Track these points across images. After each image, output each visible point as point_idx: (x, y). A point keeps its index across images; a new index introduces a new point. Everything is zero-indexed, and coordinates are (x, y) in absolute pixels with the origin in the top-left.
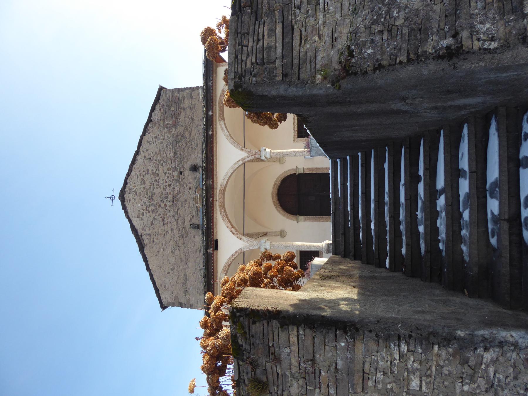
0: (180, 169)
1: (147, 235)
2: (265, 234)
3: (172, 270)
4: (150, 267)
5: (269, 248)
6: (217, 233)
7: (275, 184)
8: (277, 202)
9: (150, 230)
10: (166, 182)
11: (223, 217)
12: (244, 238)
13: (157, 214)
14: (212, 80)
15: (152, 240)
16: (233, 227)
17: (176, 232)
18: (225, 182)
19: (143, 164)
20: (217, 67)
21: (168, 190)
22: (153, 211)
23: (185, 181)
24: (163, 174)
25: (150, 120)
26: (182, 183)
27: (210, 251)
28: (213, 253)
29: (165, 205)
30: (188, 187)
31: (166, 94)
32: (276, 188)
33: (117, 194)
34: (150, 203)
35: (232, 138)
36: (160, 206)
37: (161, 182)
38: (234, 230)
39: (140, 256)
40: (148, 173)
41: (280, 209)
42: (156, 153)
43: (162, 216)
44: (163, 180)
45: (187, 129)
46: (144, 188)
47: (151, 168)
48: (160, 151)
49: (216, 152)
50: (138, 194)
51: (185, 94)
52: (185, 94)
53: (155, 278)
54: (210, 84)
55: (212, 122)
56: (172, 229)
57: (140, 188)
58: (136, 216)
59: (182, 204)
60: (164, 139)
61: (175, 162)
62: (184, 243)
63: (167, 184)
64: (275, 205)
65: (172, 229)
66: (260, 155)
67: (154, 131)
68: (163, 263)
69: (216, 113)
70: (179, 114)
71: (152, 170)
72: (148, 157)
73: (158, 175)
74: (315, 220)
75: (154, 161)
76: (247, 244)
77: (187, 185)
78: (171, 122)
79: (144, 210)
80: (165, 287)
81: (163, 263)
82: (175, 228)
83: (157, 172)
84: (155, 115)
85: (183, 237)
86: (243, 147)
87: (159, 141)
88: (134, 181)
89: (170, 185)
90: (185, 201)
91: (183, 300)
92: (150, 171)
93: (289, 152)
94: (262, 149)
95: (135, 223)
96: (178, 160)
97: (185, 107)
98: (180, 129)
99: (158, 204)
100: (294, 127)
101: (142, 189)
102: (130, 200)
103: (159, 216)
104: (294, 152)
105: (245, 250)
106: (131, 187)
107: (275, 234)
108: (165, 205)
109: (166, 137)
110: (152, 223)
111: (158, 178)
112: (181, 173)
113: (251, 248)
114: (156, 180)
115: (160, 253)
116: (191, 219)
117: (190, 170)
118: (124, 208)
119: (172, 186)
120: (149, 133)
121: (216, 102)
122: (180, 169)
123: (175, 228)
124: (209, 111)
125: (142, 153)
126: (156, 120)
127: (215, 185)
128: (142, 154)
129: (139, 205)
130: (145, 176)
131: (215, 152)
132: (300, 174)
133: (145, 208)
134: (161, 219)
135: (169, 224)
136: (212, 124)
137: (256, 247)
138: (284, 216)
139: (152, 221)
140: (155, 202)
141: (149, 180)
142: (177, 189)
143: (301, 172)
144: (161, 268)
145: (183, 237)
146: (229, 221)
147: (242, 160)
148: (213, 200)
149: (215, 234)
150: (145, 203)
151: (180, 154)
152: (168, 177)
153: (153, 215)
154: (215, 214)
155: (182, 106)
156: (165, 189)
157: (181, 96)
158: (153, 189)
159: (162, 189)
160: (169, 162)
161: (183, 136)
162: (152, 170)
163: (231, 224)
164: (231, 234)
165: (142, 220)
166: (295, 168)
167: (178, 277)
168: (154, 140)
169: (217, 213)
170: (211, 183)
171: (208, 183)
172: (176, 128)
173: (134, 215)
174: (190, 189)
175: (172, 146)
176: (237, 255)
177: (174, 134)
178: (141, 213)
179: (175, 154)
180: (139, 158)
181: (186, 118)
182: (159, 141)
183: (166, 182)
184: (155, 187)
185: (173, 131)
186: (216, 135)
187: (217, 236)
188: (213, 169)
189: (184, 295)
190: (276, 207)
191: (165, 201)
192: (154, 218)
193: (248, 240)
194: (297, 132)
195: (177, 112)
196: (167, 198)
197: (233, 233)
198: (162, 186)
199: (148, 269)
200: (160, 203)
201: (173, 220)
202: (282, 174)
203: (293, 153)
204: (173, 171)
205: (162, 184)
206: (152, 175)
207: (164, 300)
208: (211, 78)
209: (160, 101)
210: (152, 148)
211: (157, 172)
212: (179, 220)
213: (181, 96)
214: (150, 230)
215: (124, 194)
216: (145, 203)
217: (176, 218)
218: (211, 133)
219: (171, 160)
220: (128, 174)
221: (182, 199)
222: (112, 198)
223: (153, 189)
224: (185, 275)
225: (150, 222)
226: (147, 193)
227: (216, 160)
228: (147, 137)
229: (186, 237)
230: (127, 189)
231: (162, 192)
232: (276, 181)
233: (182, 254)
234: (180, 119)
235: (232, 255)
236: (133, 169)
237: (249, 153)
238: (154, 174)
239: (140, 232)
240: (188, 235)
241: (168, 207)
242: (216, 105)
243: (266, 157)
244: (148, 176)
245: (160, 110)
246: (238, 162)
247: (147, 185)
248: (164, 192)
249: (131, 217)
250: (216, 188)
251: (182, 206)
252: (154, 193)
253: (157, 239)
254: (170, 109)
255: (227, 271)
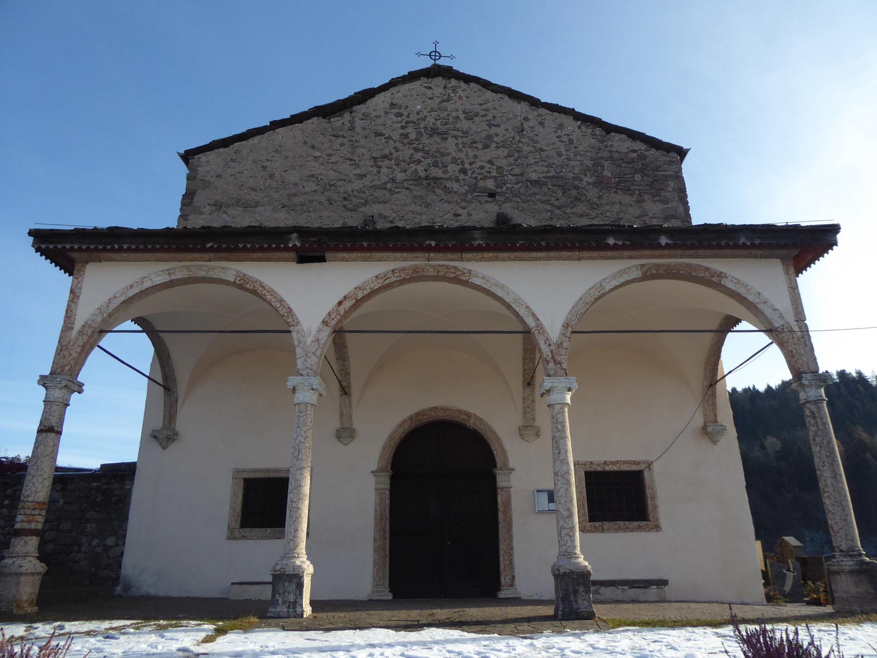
0: (500, 194)
1: (352, 122)
2: (345, 391)
3: (271, 176)
4: (280, 130)
5: (296, 401)
6: (343, 260)
7: (468, 414)
8: (425, 419)
9: (364, 129)
10: (471, 164)
11: (385, 276)
12: (328, 330)
13: (398, 145)
14: (753, 246)
15: (340, 133)
16: (358, 302)
17: (357, 184)
18: (478, 281)
19: (511, 116)
20: (784, 259)
21: (453, 169)
22: (406, 136)
23: (473, 205)
24: (489, 158)
25: (609, 129)
26: (470, 197)
27: (294, 241)
28: (287, 249)
29: (419, 162)
30: (460, 211)
31: (671, 163)
32: (461, 419)
33: (442, 62)
34: (423, 131)
35: (596, 300)
36: (416, 150)
37: (471, 153)
38: (348, 304)
39: (305, 108)
40: (490, 125)
41: (407, 427)
42: (536, 142)
43: (395, 155)
44: (475, 157)
45: (593, 209)
46: (457, 117)
47: (501, 133)
48: (542, 150)
49: (557, 259)
50: (444, 104)
51: (674, 204)
52: (674, 204)
53: (256, 140)
54: (742, 240)
55: (642, 247)
56: (365, 176)
57: (457, 110)
58: (395, 101)
59: (421, 197)
60: (569, 159)
61: (517, 183)
62: (330, 201)
63: (467, 166)
64: (417, 414)
65: (365, 176)
66: (555, 375)
67: (586, 139)
68: (287, 157)
69: (662, 257)
70: (628, 191)
71: (497, 135)
72: (526, 125)
73: (486, 147)
74: (379, 518)
75: (517, 138)
76: (309, 340)
77: (464, 208)
78: (606, 173)
79: (408, 116)
80: (232, 160)
81: (287, 157)
82: (367, 182)
83: (494, 145)
84: (620, 140)
85: (345, 199)
86: (572, 330)
87: (562, 149)
88: (473, 97)
89: (464, 171)
90: (428, 205)
91: (199, 199)
92: (494, 130)
93: (566, 458)
94: (573, 381)
95: (380, 100)
96: (523, 190)
97: (644, 205)
98: (592, 193)
99: (420, 147)
100: (612, 463)
101: (454, 114)
102: (430, 88)
103: (395, 148)
104: (568, 472)
105: (294, 334)
106: (460, 91)
107: (345, 414)
108: (419, 162)
109: (572, 163)
110: (378, 134)
111: (480, 146)
112: (492, 195)
113: (299, 351)
114: (475, 142)
115: (310, 151)
116: (385, 217)
117: (499, 215)
118: (413, 76)
119: (462, 177)
120: (579, 127)
121: (689, 257)
122: (500, 194)
123: (367, 182)
124: (670, 238)
125: (535, 113)
126: (609, 143)
127: (469, 255)
128: (533, 114)
129: (419, 107)
130: (485, 119)
131: (557, 254)
132: (493, 478)
133: (411, 119)
134: (387, 152)
135: (375, 170)
136: (634, 246)
137: (300, 364)
138: (391, 438)
139: (382, 135)
140: (425, 140)
141: (474, 128)
142: (455, 186)
143: (501, 481)
144: (277, 150)
145: (345, 199)
146: (373, 293)
147: (539, 325)
148: (429, 249)
149: (340, 255)
150: (424, 119)
151: (534, 194)
152: (482, 167)
153: (396, 136)
154: (392, 255)
155: (646, 197)
156: (454, 161)
157: (668, 194)
158: (456, 137)
159: (454, 154)
160: (517, 171)
161: (577, 199)
162: (497, 135)
163: (366, 298)
164: (340, 297)
165: (386, 113)
166: (511, 466)
167: (253, 189)
168: (565, 139)
169: (396, 259)
170: (476, 243)
171: (477, 234)
172: (595, 184)
173: (396, 96)
174: (456, 215)
175: (553, 177)
176: (283, 312)
177: (582, 180)
178: (402, 111)
179: (536, 183)
180: (524, 106)
181: (618, 206)
182: (562, 149)
183: (471, 164)
184: (460, 140)
185: (588, 179)
186: (602, 258)
187: (335, 260)
188: (514, 249)
189: (212, 202)
190: (411, 418)
191: (429, 161)
192: (390, 138)
193: (322, 341)
194: (599, 469)
195: (632, 188)
196: (436, 165)
197: (340, 303)
198: (462, 155)
199: (276, 125)
200: (423, 150)
201: (385, 179)
202: (494, 433)
203: (564, 469)
204: (495, 178)
205: (467, 155)
206: (485, 133)
207: (203, 157)
208: (757, 242)
209: (653, 151)
210: (547, 133)
211: (494, 145)
212: (385, 192)
213: (668, 194)
214: (364, 129)
215: (444, 76)
216: (424, 119)
217: (389, 186)
218: (611, 241)
219: (522, 175)
220: (486, 85)
221: (431, 197)
222: (435, 54)
223: (456, 137)
224: (257, 204)
225: (382, 129)
226: (447, 124)
227: (536, 259)
228: (571, 125)
229: (345, 206)
230: (454, 82)
231: (448, 154)
232: (478, 419)
233: (305, 197)
234: (616, 193)
235: (281, 301)
236: (499, 95)
237: (560, 345)
238: (490, 138)
239: (360, 109)
240: (350, 210)
241: (413, 167)
242: (682, 257)
243: (548, 391)
244: (484, 125)
245: (634, 151)
246: (534, 315)
247: (465, 125)
248: (449, 159)
249: (393, 90)
250: (462, 259)
251: (415, 197)
252: (445, 139)
253: (342, 145)
254: (637, 171)
255: (241, 287)
